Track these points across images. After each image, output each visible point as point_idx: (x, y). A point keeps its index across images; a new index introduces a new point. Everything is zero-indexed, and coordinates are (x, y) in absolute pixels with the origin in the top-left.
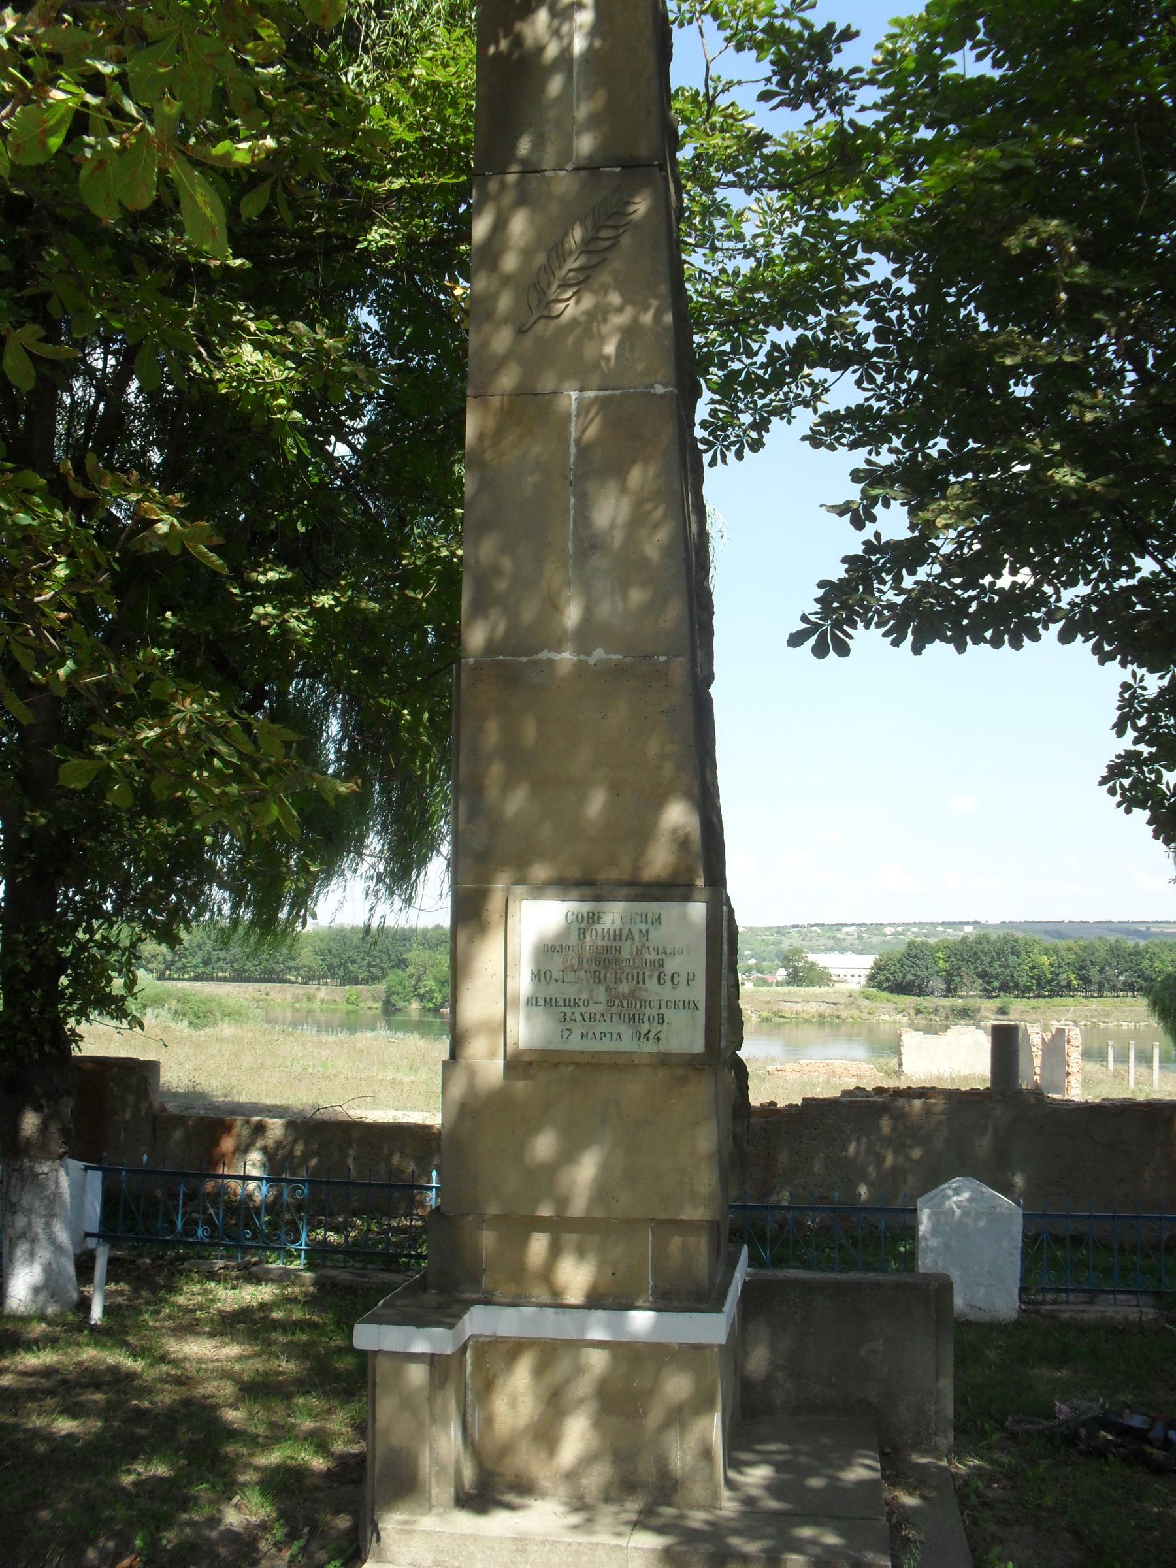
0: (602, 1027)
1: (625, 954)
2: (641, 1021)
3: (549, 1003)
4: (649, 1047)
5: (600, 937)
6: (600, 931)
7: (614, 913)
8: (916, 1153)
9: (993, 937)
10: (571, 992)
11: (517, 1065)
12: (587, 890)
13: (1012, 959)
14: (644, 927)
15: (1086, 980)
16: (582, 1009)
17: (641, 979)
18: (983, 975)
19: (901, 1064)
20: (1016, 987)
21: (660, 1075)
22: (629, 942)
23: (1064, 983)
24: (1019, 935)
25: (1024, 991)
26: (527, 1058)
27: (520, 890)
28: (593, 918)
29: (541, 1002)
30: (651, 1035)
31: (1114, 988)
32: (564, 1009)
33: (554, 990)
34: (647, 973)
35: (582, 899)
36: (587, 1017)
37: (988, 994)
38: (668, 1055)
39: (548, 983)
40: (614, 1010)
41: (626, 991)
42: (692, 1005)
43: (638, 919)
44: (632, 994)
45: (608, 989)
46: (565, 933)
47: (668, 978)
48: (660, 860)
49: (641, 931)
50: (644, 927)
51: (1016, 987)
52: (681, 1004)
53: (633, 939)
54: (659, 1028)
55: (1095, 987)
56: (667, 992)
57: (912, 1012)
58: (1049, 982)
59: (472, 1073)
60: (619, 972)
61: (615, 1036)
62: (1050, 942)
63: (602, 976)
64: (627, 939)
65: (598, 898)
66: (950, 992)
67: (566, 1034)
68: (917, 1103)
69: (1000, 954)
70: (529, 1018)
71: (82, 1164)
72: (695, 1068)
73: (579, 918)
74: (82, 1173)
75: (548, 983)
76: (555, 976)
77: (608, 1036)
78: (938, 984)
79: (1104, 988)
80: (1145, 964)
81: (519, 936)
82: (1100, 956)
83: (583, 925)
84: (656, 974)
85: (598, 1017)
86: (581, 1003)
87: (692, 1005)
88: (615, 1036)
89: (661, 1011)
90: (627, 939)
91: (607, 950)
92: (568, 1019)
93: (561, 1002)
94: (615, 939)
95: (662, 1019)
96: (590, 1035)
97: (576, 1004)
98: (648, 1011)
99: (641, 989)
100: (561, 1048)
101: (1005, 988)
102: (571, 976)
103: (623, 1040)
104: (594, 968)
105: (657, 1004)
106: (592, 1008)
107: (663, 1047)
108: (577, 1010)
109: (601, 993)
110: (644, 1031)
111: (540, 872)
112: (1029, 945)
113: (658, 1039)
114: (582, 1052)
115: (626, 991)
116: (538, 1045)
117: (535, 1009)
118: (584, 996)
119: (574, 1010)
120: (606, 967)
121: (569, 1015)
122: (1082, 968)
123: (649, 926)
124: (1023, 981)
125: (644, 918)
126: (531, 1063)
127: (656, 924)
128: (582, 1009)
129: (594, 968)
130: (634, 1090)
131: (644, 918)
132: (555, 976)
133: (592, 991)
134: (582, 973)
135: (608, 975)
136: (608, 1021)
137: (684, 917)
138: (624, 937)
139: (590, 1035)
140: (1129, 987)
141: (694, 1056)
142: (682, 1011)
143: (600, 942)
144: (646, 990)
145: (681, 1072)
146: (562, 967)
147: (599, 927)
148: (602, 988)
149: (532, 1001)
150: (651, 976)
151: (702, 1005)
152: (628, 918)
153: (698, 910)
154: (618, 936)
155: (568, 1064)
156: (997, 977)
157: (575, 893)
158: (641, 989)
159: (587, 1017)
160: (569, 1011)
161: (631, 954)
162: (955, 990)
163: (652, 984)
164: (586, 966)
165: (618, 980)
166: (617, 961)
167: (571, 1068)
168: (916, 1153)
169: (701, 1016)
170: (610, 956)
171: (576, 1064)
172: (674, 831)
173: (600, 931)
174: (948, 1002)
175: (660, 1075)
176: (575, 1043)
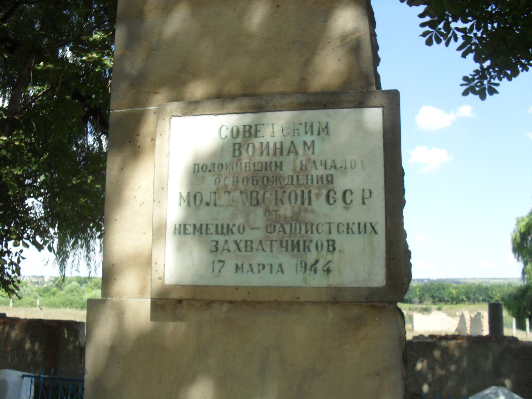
0: (260, 258)
1: (287, 170)
2: (307, 249)
3: (200, 230)
4: (318, 280)
5: (258, 152)
6: (257, 145)
7: (276, 125)
8: (453, 368)
9: (436, 284)
10: (224, 216)
11: (166, 303)
12: (246, 102)
13: (442, 291)
14: (309, 139)
15: (469, 298)
16: (237, 237)
17: (306, 199)
18: (433, 297)
19: (413, 327)
20: (444, 301)
21: (331, 316)
22: (292, 156)
23: (461, 299)
24: (445, 284)
25: (447, 302)
26: (175, 295)
27: (174, 106)
28: (250, 132)
29: (190, 229)
30: (319, 266)
31: (479, 301)
32: (215, 237)
33: (205, 215)
34: (314, 191)
35: (241, 111)
36: (242, 245)
37: (434, 303)
38: (340, 290)
39: (198, 207)
40: (274, 236)
41: (289, 213)
42: (369, 228)
43: (302, 130)
44: (296, 218)
45: (267, 211)
46: (221, 150)
47: (339, 196)
48: (330, 67)
49: (305, 143)
50: (309, 139)
51: (444, 301)
52: (355, 228)
53: (296, 153)
54: (329, 257)
55: (472, 300)
56: (338, 214)
57: (408, 310)
58: (456, 299)
59: (120, 313)
60: (280, 192)
61: (275, 268)
62: (455, 285)
63: (260, 197)
64: (289, 152)
65: (258, 109)
66: (421, 302)
67: (218, 266)
68: (453, 343)
69: (438, 289)
70: (180, 247)
71: (20, 373)
72: (373, 307)
73: (235, 133)
74: (20, 379)
75: (198, 207)
76: (206, 199)
77: (268, 268)
78: (417, 300)
79: (475, 301)
80: (490, 292)
81: (168, 156)
82: (474, 289)
83: (239, 140)
84: (324, 192)
85: (255, 245)
86: (235, 229)
87: (369, 228)
88: (275, 268)
89: (332, 237)
90: (289, 152)
91: (267, 166)
92: (220, 249)
93: (212, 229)
94: (275, 154)
95: (332, 246)
96: (246, 267)
97: (230, 231)
98: (315, 237)
99: (306, 210)
100: (212, 283)
101: (440, 301)
102: (224, 199)
103: (284, 273)
104: (251, 187)
105: (326, 227)
106: (249, 235)
107: (334, 280)
108: (231, 238)
109: (258, 217)
110: (310, 261)
111: (198, 90)
112: (448, 286)
113: (328, 271)
114: (237, 288)
115: (289, 213)
116: (189, 279)
117: (184, 238)
118: (240, 221)
119: (227, 237)
120: (265, 186)
121: (221, 245)
122: (467, 294)
123: (315, 137)
124: (446, 299)
125: (310, 128)
126: (180, 301)
127: (323, 135)
128: (237, 237)
129: (251, 187)
130: (301, 333)
131: (310, 128)
132: (206, 199)
133: (247, 215)
134: (236, 195)
135: (267, 195)
136: (267, 249)
137: (360, 126)
138: (285, 152)
139: (246, 267)
140: (484, 300)
141: (373, 291)
142: (357, 235)
143: (257, 158)
144: (312, 212)
145: (355, 311)
146: (214, 188)
147: (257, 142)
148: (260, 211)
149: (182, 230)
150: (318, 196)
151: (381, 228)
152: (293, 129)
153: (374, 116)
154: (280, 150)
155: (222, 302)
156: (437, 297)
157: (233, 106)
158: (306, 210)
159: (242, 245)
160: (221, 239)
161: (294, 170)
162: (423, 302)
163: (319, 205)
164: (241, 186)
165: (278, 201)
166: (278, 178)
167: (225, 308)
168: (453, 368)
169: (380, 240)
170: (269, 173)
171: (231, 302)
172: (344, 38)
173: (257, 145)
174: (420, 306)
175: (331, 316)
176: (229, 278)
